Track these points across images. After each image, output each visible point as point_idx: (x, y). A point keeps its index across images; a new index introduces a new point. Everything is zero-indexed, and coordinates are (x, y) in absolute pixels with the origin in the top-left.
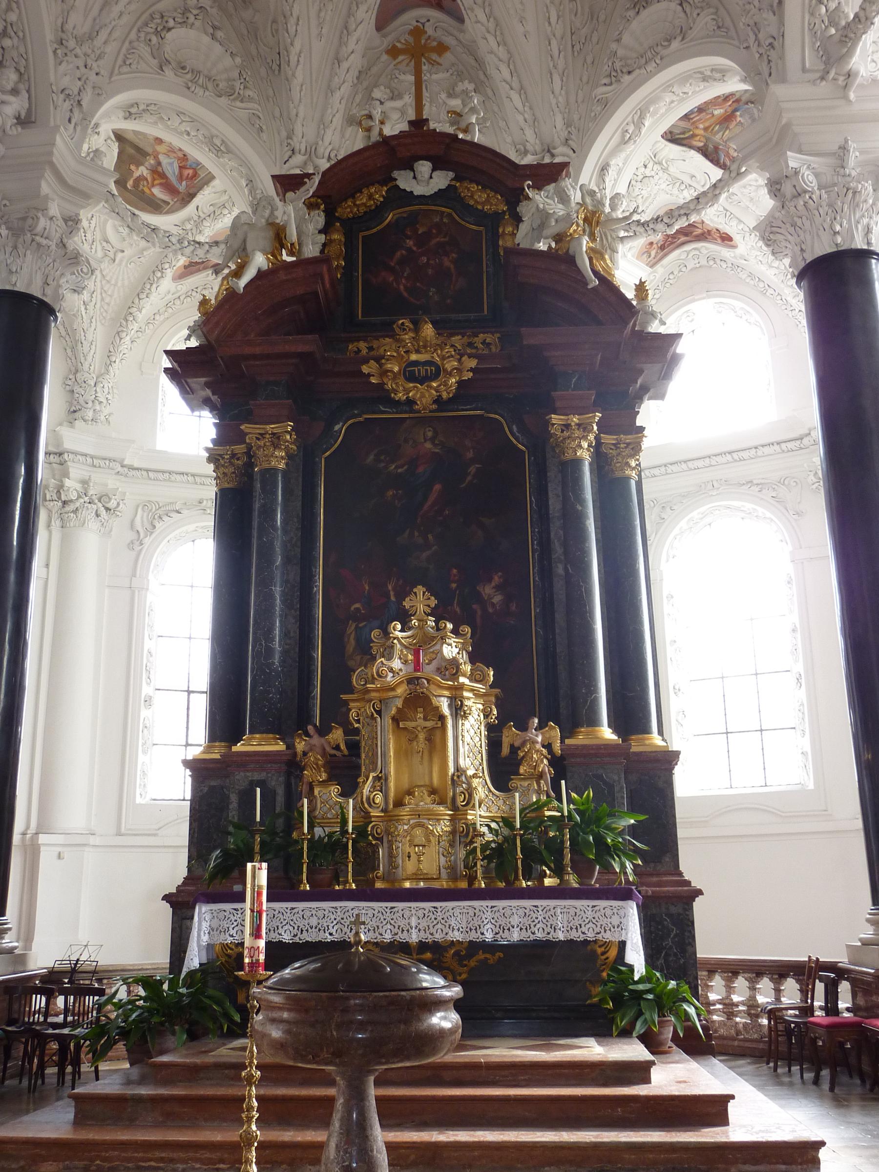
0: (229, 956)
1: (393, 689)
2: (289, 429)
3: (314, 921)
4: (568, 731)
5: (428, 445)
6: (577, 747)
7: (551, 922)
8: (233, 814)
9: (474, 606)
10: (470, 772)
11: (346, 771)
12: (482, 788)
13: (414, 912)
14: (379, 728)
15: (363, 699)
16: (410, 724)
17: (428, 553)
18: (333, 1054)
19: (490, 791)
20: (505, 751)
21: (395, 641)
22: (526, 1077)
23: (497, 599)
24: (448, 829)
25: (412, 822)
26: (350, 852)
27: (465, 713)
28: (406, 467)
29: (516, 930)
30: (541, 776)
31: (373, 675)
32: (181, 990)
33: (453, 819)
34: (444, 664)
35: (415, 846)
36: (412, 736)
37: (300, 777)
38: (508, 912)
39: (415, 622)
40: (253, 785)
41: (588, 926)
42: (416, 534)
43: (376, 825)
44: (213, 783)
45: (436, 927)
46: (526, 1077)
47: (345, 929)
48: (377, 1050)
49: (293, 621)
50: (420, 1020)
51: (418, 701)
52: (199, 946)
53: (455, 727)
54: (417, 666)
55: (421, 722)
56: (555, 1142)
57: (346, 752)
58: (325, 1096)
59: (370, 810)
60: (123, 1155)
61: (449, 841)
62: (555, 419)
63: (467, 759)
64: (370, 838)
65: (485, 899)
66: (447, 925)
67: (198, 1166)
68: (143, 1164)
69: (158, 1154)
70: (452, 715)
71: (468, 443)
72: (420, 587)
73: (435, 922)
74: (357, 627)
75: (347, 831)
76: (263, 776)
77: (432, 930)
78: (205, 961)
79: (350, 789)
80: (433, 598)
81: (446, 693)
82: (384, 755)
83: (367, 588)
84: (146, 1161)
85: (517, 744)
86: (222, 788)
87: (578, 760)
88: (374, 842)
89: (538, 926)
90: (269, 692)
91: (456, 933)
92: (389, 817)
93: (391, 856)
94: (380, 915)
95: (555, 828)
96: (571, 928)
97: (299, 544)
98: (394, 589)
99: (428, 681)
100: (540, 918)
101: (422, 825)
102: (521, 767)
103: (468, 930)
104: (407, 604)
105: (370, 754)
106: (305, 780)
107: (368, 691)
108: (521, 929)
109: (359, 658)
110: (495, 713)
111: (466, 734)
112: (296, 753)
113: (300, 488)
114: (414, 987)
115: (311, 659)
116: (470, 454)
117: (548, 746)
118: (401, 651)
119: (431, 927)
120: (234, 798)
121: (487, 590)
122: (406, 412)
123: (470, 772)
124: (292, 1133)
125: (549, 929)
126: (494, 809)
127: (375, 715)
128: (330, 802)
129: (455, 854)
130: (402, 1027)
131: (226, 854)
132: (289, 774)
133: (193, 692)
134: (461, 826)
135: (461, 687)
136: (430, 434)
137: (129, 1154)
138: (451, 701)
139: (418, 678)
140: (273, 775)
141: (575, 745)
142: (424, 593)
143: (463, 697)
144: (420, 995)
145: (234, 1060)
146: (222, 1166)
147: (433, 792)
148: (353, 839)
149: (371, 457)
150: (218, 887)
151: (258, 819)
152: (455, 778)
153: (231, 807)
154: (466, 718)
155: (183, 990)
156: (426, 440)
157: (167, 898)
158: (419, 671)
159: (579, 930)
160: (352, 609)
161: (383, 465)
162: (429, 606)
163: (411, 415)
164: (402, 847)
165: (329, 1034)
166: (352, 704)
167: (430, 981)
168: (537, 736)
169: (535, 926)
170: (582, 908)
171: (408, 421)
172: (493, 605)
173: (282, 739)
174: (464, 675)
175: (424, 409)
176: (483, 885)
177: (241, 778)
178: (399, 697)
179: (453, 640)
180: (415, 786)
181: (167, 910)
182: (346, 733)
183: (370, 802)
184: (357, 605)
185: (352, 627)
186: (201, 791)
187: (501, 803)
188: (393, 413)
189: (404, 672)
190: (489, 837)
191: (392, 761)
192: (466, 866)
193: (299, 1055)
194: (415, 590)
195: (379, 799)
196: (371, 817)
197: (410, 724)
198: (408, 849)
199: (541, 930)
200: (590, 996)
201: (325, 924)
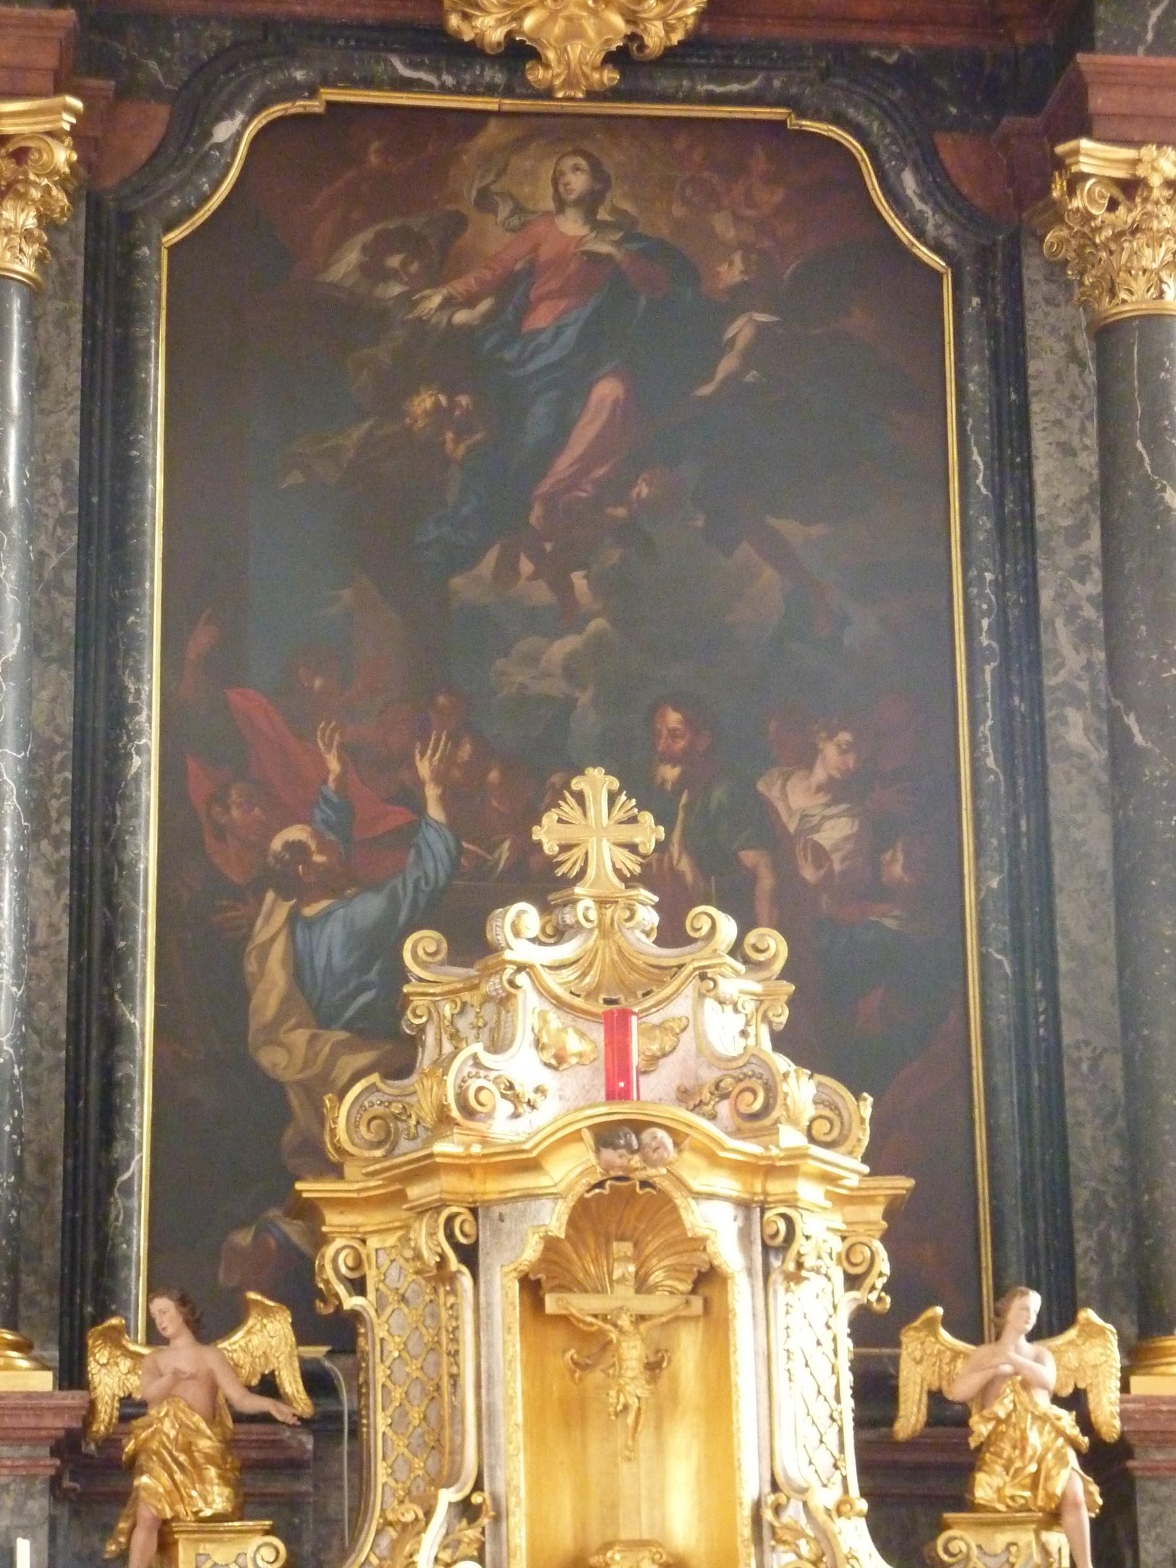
2: (67, 121)
5: (572, 225)
9: (749, 857)
14: (468, 1315)
16: (581, 1305)
17: (569, 643)
20: (911, 1416)
21: (522, 979)
23: (836, 831)
27: (800, 1265)
28: (485, 305)
34: (710, 1076)
39: (585, 907)
42: (526, 566)
49: (48, 883)
51: (623, 1208)
54: (618, 1078)
55: (624, 1298)
62: (1094, 157)
70: (750, 1272)
71: (723, 226)
72: (596, 774)
74: (293, 918)
80: (647, 818)
83: (334, 765)
97: (70, 579)
98: (440, 777)
102: (981, 1477)
104: (547, 834)
109: (300, 1037)
110: (884, 1265)
112: (92, 1406)
113: (76, 361)
115: (115, 1034)
116: (732, 272)
118: (542, 1016)
121: (796, 798)
122: (491, 90)
127: (454, 1263)
136: (578, 182)
138: (748, 1219)
142: (612, 798)
149: (351, 258)
152: (768, 1515)
156: (561, 205)
158: (625, 1095)
160: (277, 844)
161: (396, 289)
162: (633, 848)
163: (509, 104)
166: (333, 1219)
171: (493, 126)
172: (820, 855)
175: (569, 83)
178: (556, 1196)
179: (736, 983)
182: (304, 1332)
184: (297, 833)
185: (272, 917)
188: (444, 90)
194: (577, 784)
197: (581, 1305)
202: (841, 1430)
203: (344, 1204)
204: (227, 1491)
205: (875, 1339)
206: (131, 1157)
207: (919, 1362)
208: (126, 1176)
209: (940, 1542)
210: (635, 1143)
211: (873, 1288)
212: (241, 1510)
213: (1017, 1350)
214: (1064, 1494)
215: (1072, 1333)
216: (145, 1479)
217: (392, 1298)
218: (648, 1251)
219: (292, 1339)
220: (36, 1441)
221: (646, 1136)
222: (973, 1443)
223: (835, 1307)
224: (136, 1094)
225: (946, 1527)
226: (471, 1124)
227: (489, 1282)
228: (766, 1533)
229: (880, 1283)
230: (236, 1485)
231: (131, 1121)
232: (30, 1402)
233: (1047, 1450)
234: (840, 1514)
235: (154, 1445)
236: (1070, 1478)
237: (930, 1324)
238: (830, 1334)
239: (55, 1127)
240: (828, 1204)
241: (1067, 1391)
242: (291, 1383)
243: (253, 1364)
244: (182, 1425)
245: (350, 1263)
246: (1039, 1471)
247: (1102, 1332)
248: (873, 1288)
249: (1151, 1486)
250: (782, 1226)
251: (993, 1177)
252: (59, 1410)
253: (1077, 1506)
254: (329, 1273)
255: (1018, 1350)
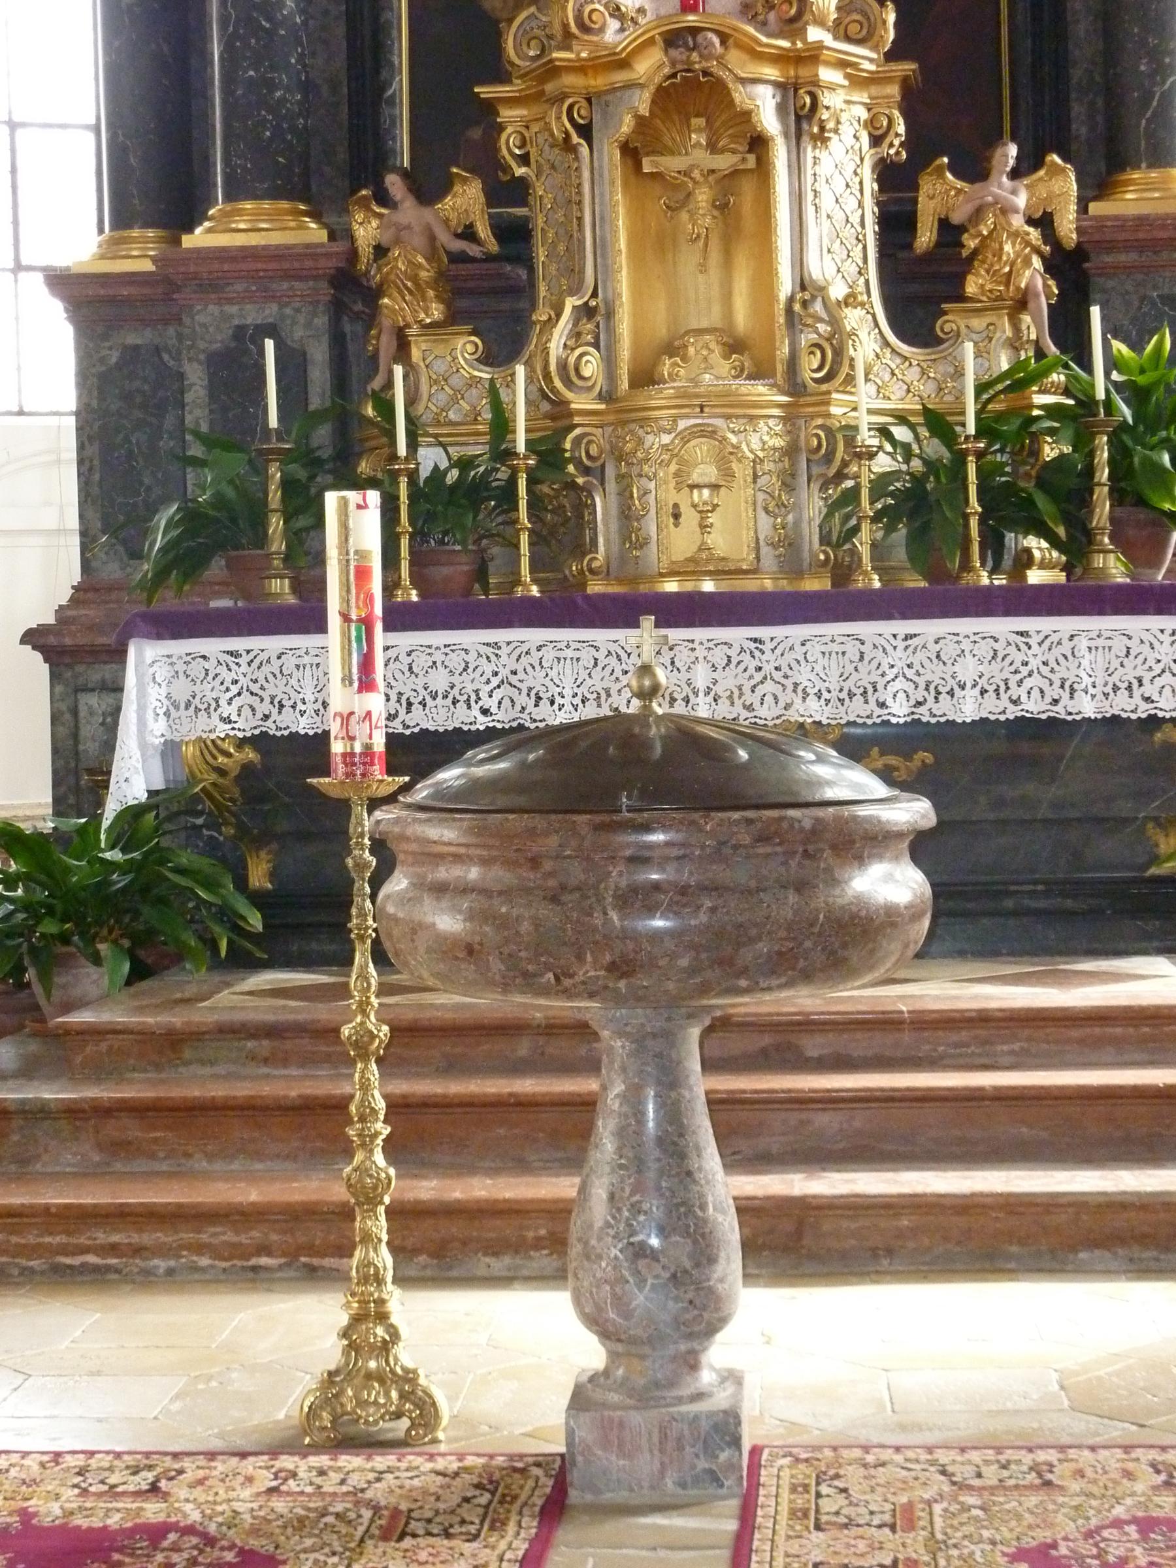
0: (221, 772)
1: (624, 64)
3: (439, 680)
4: (1098, 184)
6: (1121, 222)
7: (1062, 672)
8: (197, 411)
10: (838, 291)
11: (495, 293)
12: (868, 333)
13: (701, 652)
14: (586, 174)
15: (538, 97)
16: (671, 164)
18: (612, 968)
19: (887, 344)
20: (925, 237)
22: (1016, 1046)
24: (779, 442)
25: (682, 424)
26: (523, 505)
27: (822, 129)
29: (971, 693)
30: (1022, 303)
31: (566, 26)
32: (108, 855)
33: (790, 417)
35: (692, 487)
36: (677, 193)
37: (371, 316)
38: (949, 650)
40: (246, 341)
41: (1159, 682)
43: (587, 437)
44: (132, 339)
45: (760, 690)
46: (1016, 1046)
47: (522, 700)
48: (725, 957)
50: (835, 882)
52: (143, 746)
53: (796, 167)
55: (702, 158)
56: (1105, 1194)
57: (493, 246)
58: (511, 1095)
59: (569, 395)
60: (15, 1239)
61: (782, 474)
63: (827, 258)
64: (571, 468)
65: (889, 617)
66: (789, 683)
67: (204, 1261)
68: (68, 1261)
69: (102, 1237)
70: (786, 135)
73: (758, 677)
75: (511, 453)
76: (271, 312)
77: (749, 698)
78: (159, 785)
79: (506, 340)
81: (771, 72)
82: (602, 247)
84: (74, 1254)
85: (957, 218)
86: (157, 350)
87: (1123, 258)
88: (580, 481)
89: (1028, 683)
90: (272, 86)
91: (813, 704)
92: (621, 411)
93: (628, 515)
94: (613, 661)
95: (1069, 433)
96: (1116, 689)
99: (724, 38)
100: (1034, 663)
101: (710, 433)
103: (844, 695)
105: (561, 248)
106: (386, 322)
107: (552, 71)
108: (983, 692)
110: (901, 128)
111: (821, 186)
114: (818, 797)
117: (1044, 222)
119: (746, 689)
120: (196, 376)
123: (838, 291)
124: (434, 1183)
125: (1055, 692)
126: (897, 390)
127: (575, 139)
128: (455, 381)
129: (797, 507)
130: (792, 898)
131: (192, 518)
132: (338, 308)
133: (23, 125)
134: (811, 435)
135: (813, 56)
137: (31, 1239)
138: (784, 97)
139: (694, 31)
140: (298, 310)
141: (1116, 218)
143: (816, 82)
144: (838, 819)
145: (270, 1018)
146: (264, 1261)
147: (734, 346)
148: (530, 471)
150: (168, 600)
151: (273, 421)
152: (797, 307)
153: (189, 397)
154: (825, 140)
155: (115, 855)
157: (33, 637)
159: (1137, 693)
164: (658, 490)
165: (598, 920)
166: (507, 114)
167: (847, 782)
168: (1014, 192)
169: (1020, 683)
170: (1147, 637)
173: (316, 215)
174: (820, 22)
176: (877, 584)
177: (212, 323)
178: (642, 86)
180: (687, 333)
181: (37, 667)
183: (570, 374)
186: (102, 360)
187: (913, 374)
189: (650, 16)
190: (883, 463)
191: (622, 270)
192: (825, 540)
193: (521, 978)
195: (592, 366)
196: (571, 414)
197: (671, 164)
198: (671, 496)
199: (1035, 693)
200: (1155, 859)
201: (470, 688)
202: (865, 247)
203: (512, 102)
204: (441, 306)
205: (896, 183)
206: (393, 77)
207: (932, 198)
208: (390, 92)
209: (939, 322)
210: (691, 43)
211: (891, 145)
212: (453, 318)
213: (1001, 186)
214: (1027, 287)
215: (1042, 173)
216: (386, 300)
217: (546, 167)
218: (718, 124)
219: (482, 199)
220: (315, 278)
221: (700, 38)
222: (965, 253)
223: (862, 159)
224: (395, 33)
225: (945, 313)
226: (586, 37)
227: (601, 151)
228: (796, 320)
229: (897, 142)
230: (448, 304)
231: (391, 52)
232: (309, 251)
233: (1018, 255)
234: (847, 305)
235: (392, 277)
236: (1032, 276)
237: (939, 171)
238: (857, 180)
239: (340, 62)
240: (846, 83)
241: (1038, 215)
242: (483, 231)
243: (459, 218)
244: (410, 262)
245: (518, 143)
246: (1011, 272)
247: (1063, 170)
248: (891, 145)
249: (1101, 280)
250: (808, 100)
251: (1012, 62)
252: (328, 255)
253: (1037, 295)
254: (505, 152)
255: (1000, 186)
